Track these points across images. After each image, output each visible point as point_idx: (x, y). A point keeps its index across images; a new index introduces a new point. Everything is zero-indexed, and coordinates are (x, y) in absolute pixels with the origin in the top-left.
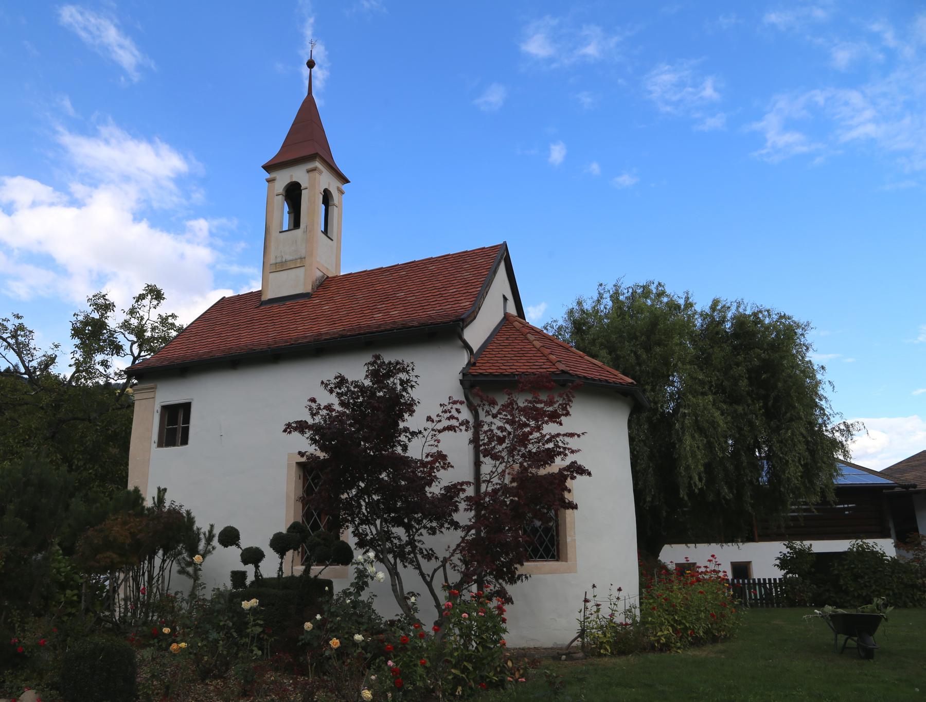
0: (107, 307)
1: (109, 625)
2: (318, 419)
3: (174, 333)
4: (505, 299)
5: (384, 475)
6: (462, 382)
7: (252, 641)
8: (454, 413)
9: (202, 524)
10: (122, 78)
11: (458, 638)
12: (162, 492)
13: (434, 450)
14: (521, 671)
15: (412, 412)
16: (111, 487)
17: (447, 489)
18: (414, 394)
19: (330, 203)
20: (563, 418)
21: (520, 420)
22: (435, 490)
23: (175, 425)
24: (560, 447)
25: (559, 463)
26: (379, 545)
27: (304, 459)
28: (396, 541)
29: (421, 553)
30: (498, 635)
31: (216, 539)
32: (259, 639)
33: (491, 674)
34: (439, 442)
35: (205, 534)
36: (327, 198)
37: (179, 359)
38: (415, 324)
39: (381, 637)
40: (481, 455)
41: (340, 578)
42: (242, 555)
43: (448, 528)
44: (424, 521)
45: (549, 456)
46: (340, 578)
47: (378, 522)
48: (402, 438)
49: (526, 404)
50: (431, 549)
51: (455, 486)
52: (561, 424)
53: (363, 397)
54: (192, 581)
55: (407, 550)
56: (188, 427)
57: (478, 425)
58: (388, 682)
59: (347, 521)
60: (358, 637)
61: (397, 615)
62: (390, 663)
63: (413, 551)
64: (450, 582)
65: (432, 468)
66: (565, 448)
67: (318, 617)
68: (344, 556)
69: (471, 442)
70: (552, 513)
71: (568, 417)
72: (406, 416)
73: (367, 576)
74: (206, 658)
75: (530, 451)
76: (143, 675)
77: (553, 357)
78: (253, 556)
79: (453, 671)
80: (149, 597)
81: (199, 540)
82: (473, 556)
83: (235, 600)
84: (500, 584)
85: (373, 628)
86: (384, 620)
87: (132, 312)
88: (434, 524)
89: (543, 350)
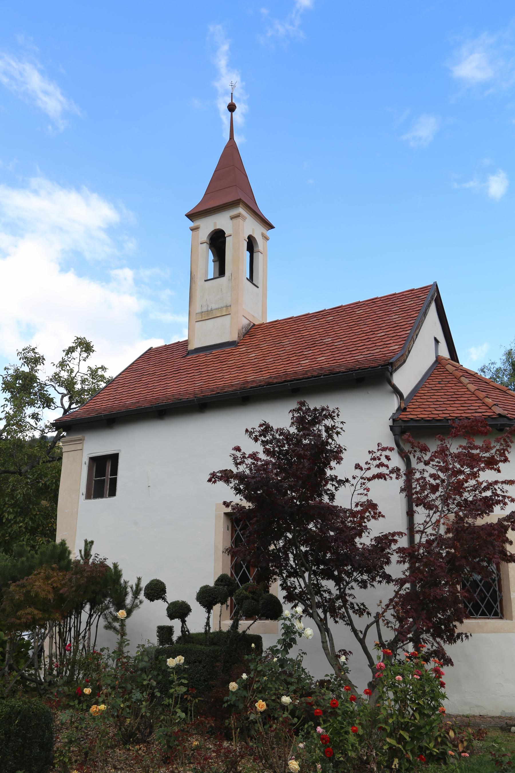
0: (37, 361)
1: (33, 685)
2: (242, 468)
3: (103, 385)
4: (437, 341)
5: (311, 526)
6: (392, 428)
7: (176, 703)
8: (384, 460)
9: (129, 577)
10: (50, 127)
11: (393, 703)
12: (89, 544)
13: (364, 499)
14: (465, 744)
15: (339, 460)
16: (41, 540)
17: (378, 539)
18: (339, 440)
19: (255, 249)
20: (501, 465)
21: (454, 467)
22: (365, 541)
23: (103, 476)
24: (498, 496)
25: (498, 513)
26: (308, 599)
27: (229, 510)
28: (326, 595)
29: (353, 608)
30: (437, 701)
31: (142, 592)
32: (181, 700)
33: (432, 745)
34: (368, 491)
35: (132, 588)
36: (251, 245)
37: (107, 410)
38: (343, 369)
39: (310, 699)
40: (414, 504)
41: (268, 633)
42: (168, 609)
43: (380, 582)
44: (355, 574)
45: (488, 505)
46: (268, 633)
47: (306, 575)
48: (329, 486)
49: (460, 450)
50: (363, 604)
51: (386, 536)
52: (499, 471)
53: (289, 445)
54: (119, 636)
55: (337, 605)
56: (116, 479)
57: (410, 472)
58: (318, 751)
59: (275, 573)
60: (286, 700)
61: (327, 675)
62: (319, 729)
63: (344, 606)
64: (384, 640)
65: (363, 518)
66: (504, 497)
67: (244, 676)
68: (273, 611)
69: (402, 490)
70: (493, 567)
71: (507, 464)
72: (333, 464)
73: (295, 633)
74: (128, 721)
75: (466, 500)
76: (61, 739)
77: (489, 401)
78: (179, 611)
79: (388, 740)
80: (75, 655)
81: (126, 594)
82: (407, 612)
83: (160, 657)
84: (438, 643)
85: (303, 691)
86: (315, 680)
87: (62, 364)
88: (365, 577)
89: (478, 393)
